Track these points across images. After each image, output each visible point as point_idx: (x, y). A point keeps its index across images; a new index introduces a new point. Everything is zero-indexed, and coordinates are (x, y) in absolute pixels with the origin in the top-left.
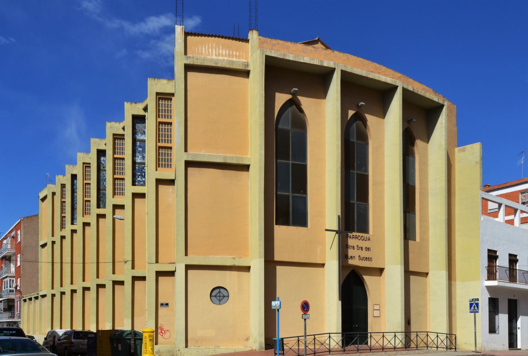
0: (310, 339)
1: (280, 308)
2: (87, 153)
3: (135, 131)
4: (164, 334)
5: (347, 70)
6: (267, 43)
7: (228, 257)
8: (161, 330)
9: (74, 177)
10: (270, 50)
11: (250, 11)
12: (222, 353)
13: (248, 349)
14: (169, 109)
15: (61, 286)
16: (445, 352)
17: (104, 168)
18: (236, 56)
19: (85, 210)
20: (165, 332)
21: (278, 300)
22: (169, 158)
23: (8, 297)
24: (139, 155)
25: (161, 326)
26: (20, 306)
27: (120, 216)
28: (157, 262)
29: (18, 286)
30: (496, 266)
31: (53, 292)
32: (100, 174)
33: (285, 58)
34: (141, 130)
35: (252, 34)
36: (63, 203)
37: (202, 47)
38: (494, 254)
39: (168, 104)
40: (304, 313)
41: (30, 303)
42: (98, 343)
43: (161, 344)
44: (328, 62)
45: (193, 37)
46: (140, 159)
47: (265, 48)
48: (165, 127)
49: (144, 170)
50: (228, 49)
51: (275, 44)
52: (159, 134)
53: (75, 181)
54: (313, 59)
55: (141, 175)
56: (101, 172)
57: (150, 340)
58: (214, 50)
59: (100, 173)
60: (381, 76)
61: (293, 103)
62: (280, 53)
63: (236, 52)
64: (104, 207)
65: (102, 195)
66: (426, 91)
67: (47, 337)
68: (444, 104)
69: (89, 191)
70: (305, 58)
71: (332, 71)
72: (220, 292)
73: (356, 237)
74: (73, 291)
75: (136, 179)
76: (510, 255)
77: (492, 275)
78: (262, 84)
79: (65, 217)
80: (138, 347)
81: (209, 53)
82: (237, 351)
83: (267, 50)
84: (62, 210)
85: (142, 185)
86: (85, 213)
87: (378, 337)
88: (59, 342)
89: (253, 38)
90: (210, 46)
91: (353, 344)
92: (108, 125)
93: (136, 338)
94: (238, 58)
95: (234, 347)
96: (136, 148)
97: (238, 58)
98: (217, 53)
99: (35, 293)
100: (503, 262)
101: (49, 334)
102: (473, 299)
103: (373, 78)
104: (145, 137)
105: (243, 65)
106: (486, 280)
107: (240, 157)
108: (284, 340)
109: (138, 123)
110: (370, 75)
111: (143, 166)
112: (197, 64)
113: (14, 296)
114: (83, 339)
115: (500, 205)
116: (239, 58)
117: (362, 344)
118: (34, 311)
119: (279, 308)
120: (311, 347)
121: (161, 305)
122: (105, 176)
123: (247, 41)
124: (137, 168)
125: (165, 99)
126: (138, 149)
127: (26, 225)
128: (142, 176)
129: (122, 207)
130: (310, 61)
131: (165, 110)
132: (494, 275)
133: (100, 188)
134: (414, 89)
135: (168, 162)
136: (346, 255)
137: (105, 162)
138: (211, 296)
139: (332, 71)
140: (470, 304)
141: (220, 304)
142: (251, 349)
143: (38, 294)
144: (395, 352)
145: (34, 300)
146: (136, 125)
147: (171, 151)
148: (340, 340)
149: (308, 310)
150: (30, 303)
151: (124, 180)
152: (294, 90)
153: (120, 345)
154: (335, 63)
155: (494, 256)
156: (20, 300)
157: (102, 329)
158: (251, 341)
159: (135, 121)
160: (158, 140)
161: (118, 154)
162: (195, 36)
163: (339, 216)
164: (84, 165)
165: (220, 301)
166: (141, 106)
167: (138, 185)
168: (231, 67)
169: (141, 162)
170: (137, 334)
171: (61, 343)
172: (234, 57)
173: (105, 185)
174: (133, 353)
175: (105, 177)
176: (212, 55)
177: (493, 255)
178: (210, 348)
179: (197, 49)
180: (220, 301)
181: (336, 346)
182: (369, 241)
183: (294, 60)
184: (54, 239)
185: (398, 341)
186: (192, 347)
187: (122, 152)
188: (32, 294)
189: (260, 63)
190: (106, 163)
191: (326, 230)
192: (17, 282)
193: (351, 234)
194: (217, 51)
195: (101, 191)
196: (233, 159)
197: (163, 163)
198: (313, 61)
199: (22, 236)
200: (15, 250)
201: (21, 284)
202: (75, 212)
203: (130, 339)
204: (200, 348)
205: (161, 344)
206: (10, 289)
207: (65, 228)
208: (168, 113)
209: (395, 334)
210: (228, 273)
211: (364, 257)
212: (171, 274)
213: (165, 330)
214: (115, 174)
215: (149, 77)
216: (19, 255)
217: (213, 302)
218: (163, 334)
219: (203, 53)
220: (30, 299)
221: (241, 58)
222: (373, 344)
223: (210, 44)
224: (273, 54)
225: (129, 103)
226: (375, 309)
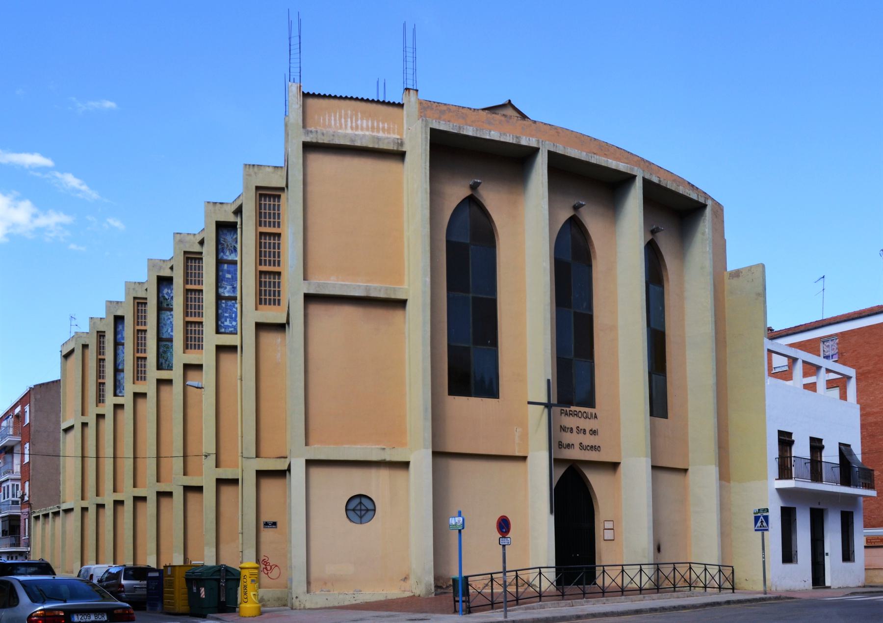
0: (511, 576)
1: (463, 528)
5: (557, 152)
6: (433, 109)
7: (374, 447)
8: (265, 565)
11: (405, 60)
12: (365, 601)
13: (408, 594)
14: (276, 212)
16: (718, 594)
17: (168, 305)
20: (271, 569)
21: (460, 515)
22: (277, 289)
23: (10, 512)
26: (29, 527)
27: (197, 383)
29: (26, 494)
30: (791, 457)
31: (85, 504)
33: (462, 133)
35: (409, 95)
36: (101, 362)
37: (330, 116)
38: (788, 437)
39: (274, 205)
40: (501, 536)
41: (45, 521)
44: (528, 139)
46: (229, 292)
47: (429, 118)
48: (270, 241)
49: (234, 309)
50: (370, 119)
51: (444, 111)
54: (505, 134)
55: (231, 317)
58: (349, 120)
60: (610, 161)
61: (472, 202)
62: (453, 125)
63: (383, 123)
64: (170, 368)
66: (678, 183)
68: (707, 203)
70: (492, 132)
71: (533, 152)
72: (361, 503)
73: (575, 413)
74: (118, 503)
76: (812, 439)
77: (786, 471)
78: (426, 173)
79: (104, 384)
82: (390, 598)
83: (432, 120)
84: (100, 373)
87: (614, 572)
90: (343, 115)
91: (577, 584)
94: (386, 133)
95: (384, 592)
97: (386, 133)
98: (354, 124)
99: (53, 506)
100: (801, 450)
102: (759, 510)
103: (598, 163)
104: (236, 256)
106: (776, 479)
107: (390, 287)
108: (470, 579)
110: (593, 158)
111: (233, 302)
112: (322, 142)
113: (20, 511)
115: (793, 360)
116: (389, 133)
117: (590, 584)
118: (53, 535)
119: (462, 528)
120: (512, 589)
121: (264, 525)
125: (270, 196)
127: (38, 396)
130: (500, 137)
131: (270, 214)
132: (789, 472)
134: (660, 181)
136: (559, 442)
138: (347, 510)
139: (533, 152)
140: (755, 517)
141: (361, 523)
142: (411, 594)
144: (642, 596)
145: (53, 518)
148: (598, 579)
149: (508, 531)
150: (45, 521)
152: (475, 182)
154: (538, 141)
155: (788, 440)
156: (29, 516)
157: (170, 564)
158: (412, 581)
161: (191, 284)
163: (549, 381)
165: (361, 517)
168: (376, 146)
172: (381, 132)
174: (223, 602)
177: (787, 439)
178: (347, 593)
179: (322, 118)
180: (361, 517)
181: (647, 584)
182: (596, 419)
183: (475, 135)
184: (85, 419)
185: (645, 579)
186: (317, 593)
187: (199, 281)
188: (49, 508)
189: (422, 141)
191: (529, 403)
192: (23, 488)
193: (568, 409)
194: (354, 121)
196: (380, 290)
197: (268, 297)
198: (505, 137)
199: (33, 415)
200: (20, 437)
201: (30, 491)
204: (331, 593)
205: (266, 588)
206: (13, 499)
207: (103, 402)
208: (274, 218)
209: (641, 567)
211: (589, 446)
212: (283, 474)
213: (271, 565)
216: (27, 445)
218: (269, 572)
219: (331, 124)
220: (46, 516)
221: (391, 132)
222: (607, 584)
223: (343, 112)
224: (443, 126)
226: (605, 528)
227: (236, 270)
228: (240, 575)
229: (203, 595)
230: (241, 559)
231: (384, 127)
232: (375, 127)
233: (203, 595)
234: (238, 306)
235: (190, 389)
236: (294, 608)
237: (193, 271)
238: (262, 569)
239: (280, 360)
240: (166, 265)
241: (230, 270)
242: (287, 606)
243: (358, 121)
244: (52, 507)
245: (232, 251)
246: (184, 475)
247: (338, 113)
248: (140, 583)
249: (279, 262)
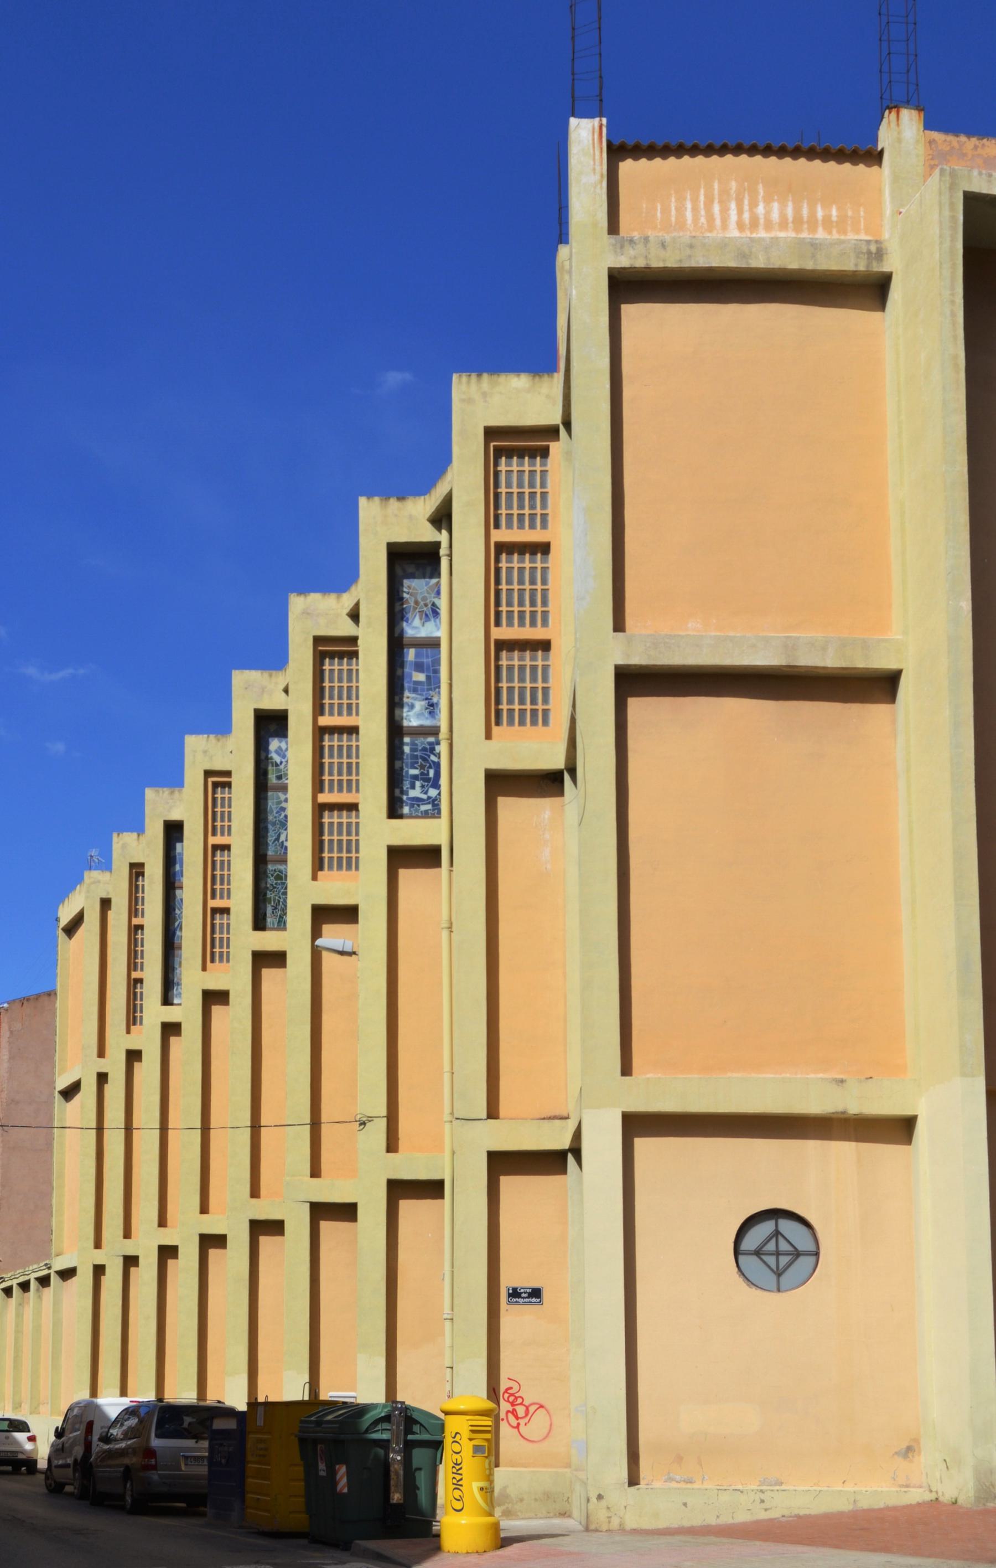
2: (219, 736)
3: (397, 608)
4: (527, 1418)
6: (965, 155)
7: (812, 1076)
8: (513, 1404)
9: (173, 831)
10: (984, 172)
12: (796, 1512)
13: (916, 1496)
14: (538, 490)
15: (127, 1234)
17: (279, 778)
18: (828, 223)
19: (213, 946)
24: (416, 699)
25: (511, 1384)
27: (342, 941)
28: (493, 1113)
31: (99, 1257)
32: (266, 804)
34: (422, 603)
35: (898, 125)
36: (135, 930)
37: (681, 200)
42: (249, 1457)
43: (512, 1464)
45: (644, 161)
46: (419, 716)
49: (433, 758)
52: (498, 593)
53: (178, 845)
55: (424, 777)
56: (270, 794)
57: (477, 1449)
58: (733, 206)
59: (266, 798)
65: (271, 880)
67: (63, 1429)
69: (226, 872)
72: (777, 1233)
74: (167, 1253)
75: (402, 792)
78: (953, 315)
79: (140, 981)
80: (422, 1479)
81: (710, 218)
85: (426, 815)
86: (213, 954)
88: (106, 1447)
89: (899, 140)
90: (716, 192)
92: (297, 604)
93: (410, 1437)
94: (834, 231)
95: (849, 1488)
96: (403, 672)
97: (834, 231)
98: (746, 216)
101: (76, 1411)
104: (438, 628)
105: (858, 254)
109: (412, 576)
111: (431, 739)
112: (661, 265)
114: (193, 1437)
118: (37, 1329)
121: (510, 1295)
122: (284, 809)
123: (875, 157)
124: (407, 749)
125: (521, 453)
126: (411, 676)
127: (18, 1026)
128: (428, 780)
129: (349, 914)
133: (266, 855)
135: (536, 704)
137: (284, 756)
138: (737, 1252)
141: (779, 1290)
142: (928, 1497)
143: (49, 1268)
145: (38, 1290)
146: (402, 585)
147: (545, 658)
150: (23, 1298)
151: (357, 733)
153: (342, 1470)
158: (928, 1458)
159: (399, 571)
160: (494, 616)
161: (331, 714)
162: (650, 158)
164: (211, 780)
165: (779, 1274)
166: (424, 507)
167: (410, 816)
168: (809, 265)
169: (421, 726)
170: (416, 1422)
171: (109, 1451)
172: (820, 229)
173: (285, 844)
175: (283, 814)
176: (725, 226)
178: (740, 1487)
180: (779, 1274)
189: (941, 229)
190: (287, 762)
194: (746, 208)
195: (270, 867)
196: (824, 649)
202: (177, 959)
203: (388, 1441)
204: (695, 1486)
205: (513, 1466)
207: (141, 1023)
210: (811, 1148)
213: (526, 1403)
214: (321, 790)
215: (457, 372)
217: (748, 1280)
218: (522, 1422)
220: (25, 1286)
223: (716, 186)
225: (377, 499)
227: (437, 662)
228: (443, 1431)
229: (342, 1484)
230: (448, 1387)
231: (830, 216)
232: (805, 219)
233: (342, 1484)
234: (443, 748)
235: (328, 960)
236: (592, 1527)
237: (336, 684)
238: (502, 1415)
239: (549, 867)
240: (276, 683)
241: (423, 663)
242: (570, 1516)
243: (756, 205)
244: (35, 1266)
245: (427, 615)
246: (312, 1176)
247: (702, 192)
248: (196, 1446)
249: (545, 614)
